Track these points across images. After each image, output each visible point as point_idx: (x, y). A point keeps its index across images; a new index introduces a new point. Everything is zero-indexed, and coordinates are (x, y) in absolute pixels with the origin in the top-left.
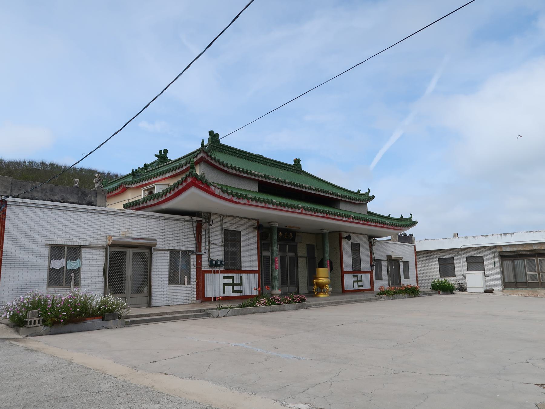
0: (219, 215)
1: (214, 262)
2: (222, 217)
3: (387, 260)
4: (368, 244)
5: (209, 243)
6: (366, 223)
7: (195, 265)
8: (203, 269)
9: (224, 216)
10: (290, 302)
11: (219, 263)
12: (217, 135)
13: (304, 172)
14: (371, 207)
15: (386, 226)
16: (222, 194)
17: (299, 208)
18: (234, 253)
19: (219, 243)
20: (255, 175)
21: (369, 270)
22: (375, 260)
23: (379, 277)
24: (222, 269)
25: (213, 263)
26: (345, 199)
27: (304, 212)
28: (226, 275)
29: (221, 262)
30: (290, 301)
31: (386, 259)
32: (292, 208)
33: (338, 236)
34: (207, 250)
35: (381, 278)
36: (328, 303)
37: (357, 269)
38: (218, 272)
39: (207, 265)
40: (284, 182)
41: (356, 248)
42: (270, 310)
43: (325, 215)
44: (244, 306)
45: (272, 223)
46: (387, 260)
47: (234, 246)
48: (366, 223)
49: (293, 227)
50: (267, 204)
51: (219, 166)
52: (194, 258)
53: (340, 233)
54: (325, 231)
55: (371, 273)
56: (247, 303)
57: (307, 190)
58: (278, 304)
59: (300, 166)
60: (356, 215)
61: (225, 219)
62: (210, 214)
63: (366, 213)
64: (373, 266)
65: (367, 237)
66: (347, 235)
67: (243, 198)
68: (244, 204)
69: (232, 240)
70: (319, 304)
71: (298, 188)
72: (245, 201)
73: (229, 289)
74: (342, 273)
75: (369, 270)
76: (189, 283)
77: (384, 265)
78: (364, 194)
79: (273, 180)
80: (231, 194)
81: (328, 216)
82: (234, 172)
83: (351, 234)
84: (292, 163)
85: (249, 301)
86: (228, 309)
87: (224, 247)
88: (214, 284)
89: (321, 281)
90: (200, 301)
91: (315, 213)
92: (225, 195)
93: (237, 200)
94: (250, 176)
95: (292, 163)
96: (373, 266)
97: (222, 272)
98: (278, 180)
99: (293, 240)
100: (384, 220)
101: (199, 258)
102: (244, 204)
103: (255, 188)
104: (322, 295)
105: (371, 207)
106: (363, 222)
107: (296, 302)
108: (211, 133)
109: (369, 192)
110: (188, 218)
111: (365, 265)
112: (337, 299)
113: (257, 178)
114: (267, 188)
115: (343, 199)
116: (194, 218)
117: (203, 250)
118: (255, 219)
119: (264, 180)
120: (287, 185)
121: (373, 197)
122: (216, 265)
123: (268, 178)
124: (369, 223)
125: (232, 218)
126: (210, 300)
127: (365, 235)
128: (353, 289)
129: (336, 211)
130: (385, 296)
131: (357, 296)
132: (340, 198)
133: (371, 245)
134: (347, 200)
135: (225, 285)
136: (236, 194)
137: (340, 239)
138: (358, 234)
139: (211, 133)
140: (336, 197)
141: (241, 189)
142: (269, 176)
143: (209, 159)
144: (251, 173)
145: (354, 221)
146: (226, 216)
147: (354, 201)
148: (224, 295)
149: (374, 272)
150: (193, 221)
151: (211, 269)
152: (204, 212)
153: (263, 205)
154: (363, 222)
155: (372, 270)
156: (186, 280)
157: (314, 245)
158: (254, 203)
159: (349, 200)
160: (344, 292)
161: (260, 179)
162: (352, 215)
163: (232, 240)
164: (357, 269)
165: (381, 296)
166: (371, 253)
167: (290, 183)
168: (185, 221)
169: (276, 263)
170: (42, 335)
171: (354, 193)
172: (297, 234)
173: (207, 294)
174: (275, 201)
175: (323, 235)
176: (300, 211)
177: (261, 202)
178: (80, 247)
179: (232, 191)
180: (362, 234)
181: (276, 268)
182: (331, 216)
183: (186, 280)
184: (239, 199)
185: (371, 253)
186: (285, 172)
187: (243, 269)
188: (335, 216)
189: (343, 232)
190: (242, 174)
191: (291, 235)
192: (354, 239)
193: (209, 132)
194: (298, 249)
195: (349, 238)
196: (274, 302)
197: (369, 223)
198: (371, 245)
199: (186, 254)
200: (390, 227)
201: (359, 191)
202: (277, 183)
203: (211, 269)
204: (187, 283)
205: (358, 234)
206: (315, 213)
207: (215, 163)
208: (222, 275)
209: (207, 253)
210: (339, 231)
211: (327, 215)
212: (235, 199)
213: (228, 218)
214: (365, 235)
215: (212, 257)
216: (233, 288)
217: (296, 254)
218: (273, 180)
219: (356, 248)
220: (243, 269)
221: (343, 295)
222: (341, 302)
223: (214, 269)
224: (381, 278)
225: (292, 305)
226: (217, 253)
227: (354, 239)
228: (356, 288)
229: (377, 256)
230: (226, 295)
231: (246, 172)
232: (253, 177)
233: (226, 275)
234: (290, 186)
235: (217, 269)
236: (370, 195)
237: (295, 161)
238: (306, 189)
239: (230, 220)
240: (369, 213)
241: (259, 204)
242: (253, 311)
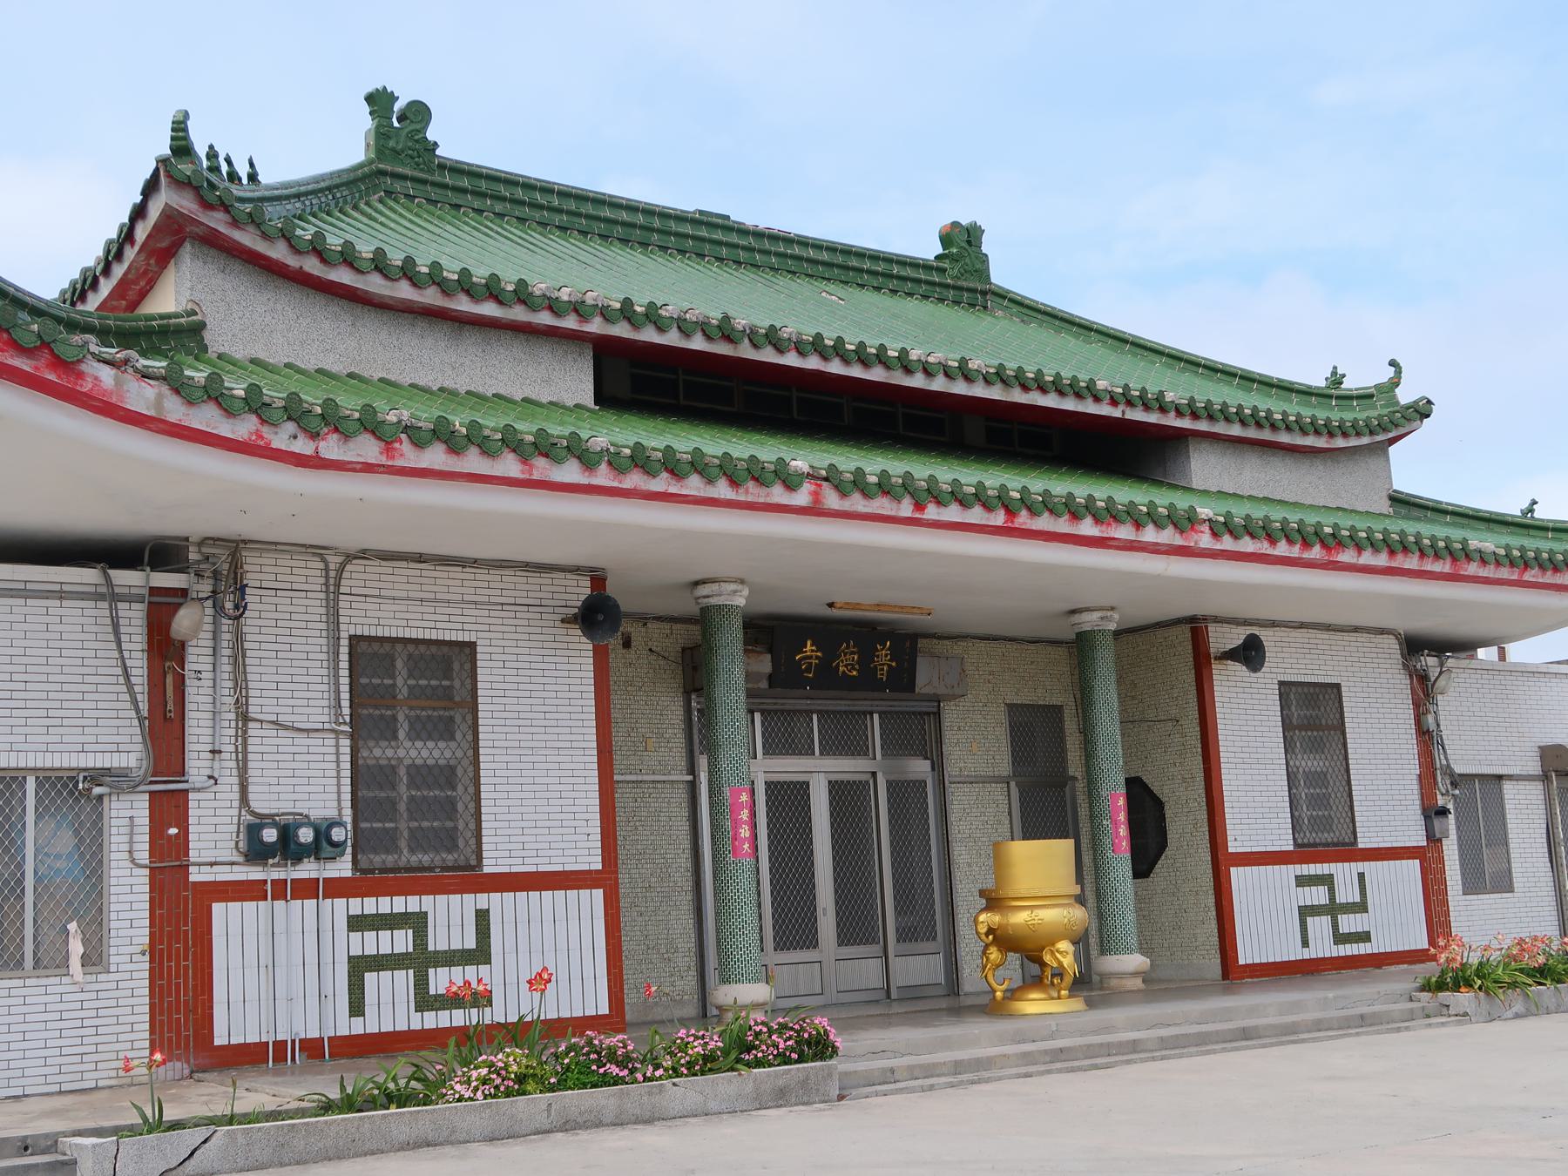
0: (317, 551)
1: (270, 835)
2: (336, 565)
3: (1545, 778)
4: (1401, 685)
5: (244, 718)
6: (1316, 552)
7: (143, 856)
8: (196, 875)
9: (350, 557)
10: (707, 1064)
11: (306, 835)
12: (419, 113)
13: (1002, 295)
14: (1415, 467)
15: (1473, 569)
16: (175, 410)
17: (790, 482)
18: (446, 775)
19: (319, 715)
20: (553, 306)
21: (1415, 836)
22: (1457, 780)
23: (1488, 876)
24: (342, 868)
25: (276, 842)
26: (1220, 428)
27: (832, 500)
28: (370, 906)
29: (322, 833)
30: (709, 1058)
31: (1534, 768)
32: (734, 483)
33: (1190, 650)
34: (229, 764)
35: (1504, 884)
36: (1027, 1058)
37: (1324, 835)
38: (306, 889)
39: (228, 853)
40: (773, 338)
41: (1313, 716)
42: (542, 1121)
43: (999, 518)
44: (349, 1104)
45: (703, 590)
46: (1545, 778)
47: (445, 731)
48: (1316, 552)
49: (879, 606)
50: (541, 462)
51: (292, 261)
52: (127, 820)
53: (1196, 627)
54: (1089, 621)
55: (1428, 856)
56: (574, 1061)
57: (939, 384)
58: (608, 1081)
59: (982, 271)
60: (1239, 511)
61: (356, 577)
62: (236, 547)
63: (1384, 507)
64: (1443, 812)
65: (1392, 646)
66: (1234, 637)
67: (1437, 556)
68: (368, 468)
69: (410, 696)
70: (958, 1067)
71: (877, 374)
72: (367, 449)
73: (1320, 926)
74: (1221, 861)
75: (1415, 836)
76: (94, 959)
77: (1525, 814)
78: (1365, 397)
79: (687, 334)
80: (255, 404)
81: (1023, 520)
82: (404, 291)
83: (1265, 635)
84: (928, 248)
85: (397, 1071)
86: (203, 1132)
87: (352, 737)
88: (280, 966)
89: (1020, 918)
90: (179, 1067)
91: (919, 507)
92: (206, 418)
93: (303, 446)
94: (519, 314)
95: (928, 248)
96: (1443, 812)
97: (336, 888)
98: (726, 331)
99: (903, 680)
100: (1456, 534)
101: (170, 810)
102: (368, 468)
103: (573, 382)
104: (1034, 1004)
105: (1415, 467)
106: (1295, 551)
107: (759, 1063)
108: (379, 101)
109: (1395, 382)
110: (87, 576)
111: (1385, 805)
112: (1109, 1029)
113: (570, 323)
114: (648, 377)
115: (1203, 426)
116: (127, 579)
117: (197, 767)
118: (576, 570)
119: (621, 330)
120: (791, 360)
121: (1421, 411)
122: (288, 848)
123: (653, 316)
124: (1347, 556)
125: (404, 569)
126: (248, 1057)
127: (1382, 631)
128: (1296, 953)
129: (1162, 499)
130: (1463, 999)
131: (1310, 999)
132: (1186, 423)
133: (1424, 692)
134: (1236, 430)
135: (360, 967)
136: (294, 412)
137: (1202, 662)
138: (1328, 628)
139: (379, 101)
140: (1153, 418)
141: (1267, 500)
142: (1092, 382)
143: (216, 221)
144: (522, 295)
145: (1227, 543)
146: (363, 555)
147: (1284, 438)
148: (358, 1027)
149: (1451, 849)
150: (113, 597)
151: (255, 873)
152: (203, 542)
153: (1382, 560)
154: (1295, 551)
155: (1434, 840)
156: (76, 948)
157: (1057, 710)
158: (435, 457)
159: (1252, 433)
160: (1232, 972)
161: (596, 326)
162: (1204, 512)
163: (410, 696)
164: (1324, 835)
165: (1444, 996)
166: (1427, 738)
167: (999, 376)
168: (61, 595)
169: (736, 824)
170: (599, 1124)
171: (1306, 393)
172: (922, 643)
173: (232, 1024)
174: (800, 464)
175: (706, 618)
176: (802, 498)
177: (487, 451)
178: (1500, 777)
179: (254, 390)
180: (1356, 629)
181: (735, 852)
182: (1044, 523)
183: (76, 948)
184: (314, 436)
185: (1427, 738)
186: (914, 308)
187: (492, 864)
188: (1075, 517)
189: (1217, 620)
190: (463, 305)
191: (883, 656)
192: (1290, 660)
193: (370, 99)
194: (949, 736)
195: (1250, 654)
196: (585, 1069)
197: (1347, 556)
198: (1424, 692)
199: (76, 791)
200: (1504, 573)
201: (1336, 379)
202: (722, 349)
203: (255, 873)
204: (86, 961)
205: (1328, 628)
206: (919, 507)
207: (261, 247)
208: (342, 908)
209: (229, 782)
210: (1192, 619)
211: (1011, 513)
212: (283, 437)
213: (375, 567)
214: (1382, 631)
215: (262, 802)
216: (421, 983)
217: (938, 767)
218: (684, 327)
219: (1313, 716)
220: (492, 864)
221: (1227, 991)
222: (1134, 1047)
223: (277, 874)
224: (1504, 884)
225: (724, 1084)
226: (308, 779)
227: (1290, 660)
228: (1322, 946)
229: (1465, 752)
230: (370, 1024)
231: (492, 290)
232: (545, 318)
233: (370, 906)
234: (813, 363)
235: (307, 870)
236: (1405, 395)
237: (946, 240)
238: (928, 372)
239: (400, 577)
240: (1402, 503)
241: (473, 462)
242: (403, 1132)
